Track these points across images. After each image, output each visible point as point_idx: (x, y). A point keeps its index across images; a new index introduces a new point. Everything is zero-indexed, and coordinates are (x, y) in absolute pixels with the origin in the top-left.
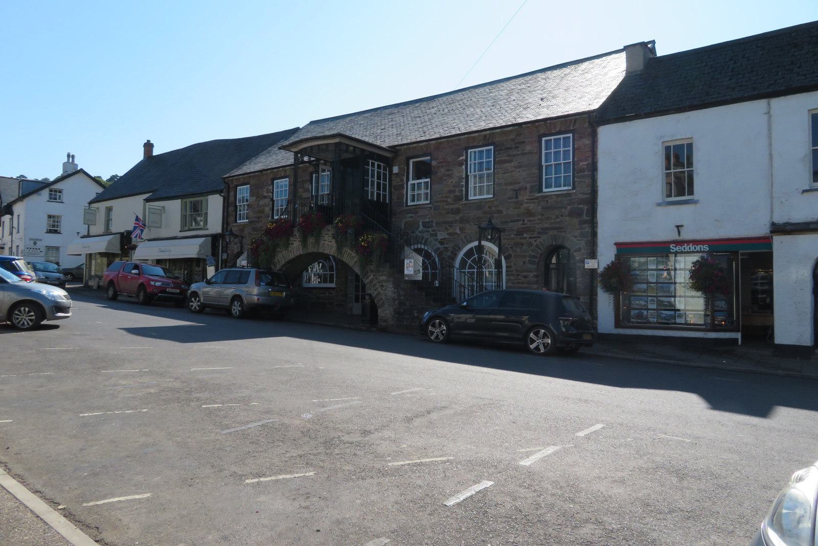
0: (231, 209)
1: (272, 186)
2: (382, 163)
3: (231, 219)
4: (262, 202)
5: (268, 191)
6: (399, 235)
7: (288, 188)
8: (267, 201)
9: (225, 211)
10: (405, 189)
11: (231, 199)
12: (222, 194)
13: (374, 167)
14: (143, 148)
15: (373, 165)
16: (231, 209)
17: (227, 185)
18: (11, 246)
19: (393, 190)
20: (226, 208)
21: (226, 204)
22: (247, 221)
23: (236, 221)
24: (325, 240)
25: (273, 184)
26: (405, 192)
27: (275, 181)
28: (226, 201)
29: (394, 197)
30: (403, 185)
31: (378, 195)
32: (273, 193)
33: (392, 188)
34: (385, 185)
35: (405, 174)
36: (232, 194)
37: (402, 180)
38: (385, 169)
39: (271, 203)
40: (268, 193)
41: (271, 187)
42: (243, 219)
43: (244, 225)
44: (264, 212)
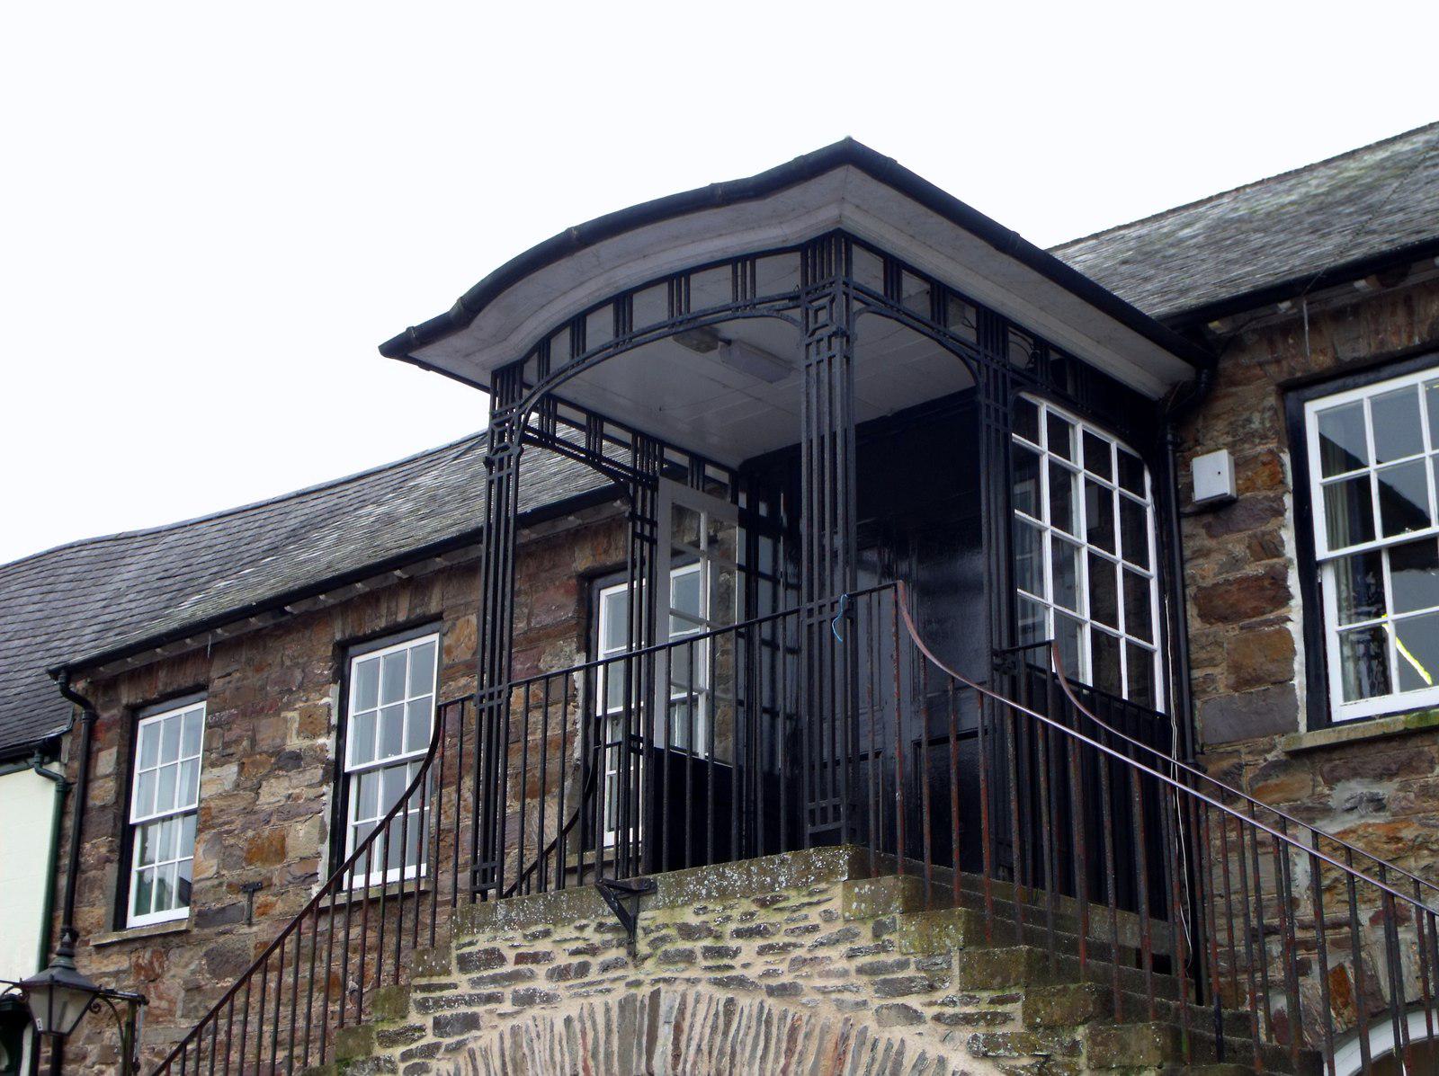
0: (98, 847)
1: (335, 689)
2: (1120, 436)
3: (94, 912)
4: (275, 792)
5: (310, 726)
6: (1275, 947)
7: (200, 755)
8: (306, 784)
9: (66, 861)
10: (1297, 602)
11: (103, 791)
12: (55, 768)
13: (1053, 466)
14: (707, 185)
15: (1060, 442)
16: (98, 847)
17: (79, 709)
18: (835, 536)
19: (1195, 625)
20: (68, 847)
21: (69, 823)
22: (184, 912)
23: (120, 921)
24: (741, 982)
25: (342, 677)
26: (1295, 627)
27: (142, 723)
28: (72, 804)
29: (1216, 677)
30: (1278, 580)
31: (1104, 647)
32: (341, 730)
33: (1192, 610)
34: (1137, 587)
35: (1288, 501)
36: (106, 762)
37: (1271, 548)
38: (1131, 479)
39: (328, 789)
40: (315, 736)
41: (331, 699)
42: (161, 906)
43: (166, 939)
44: (281, 853)
